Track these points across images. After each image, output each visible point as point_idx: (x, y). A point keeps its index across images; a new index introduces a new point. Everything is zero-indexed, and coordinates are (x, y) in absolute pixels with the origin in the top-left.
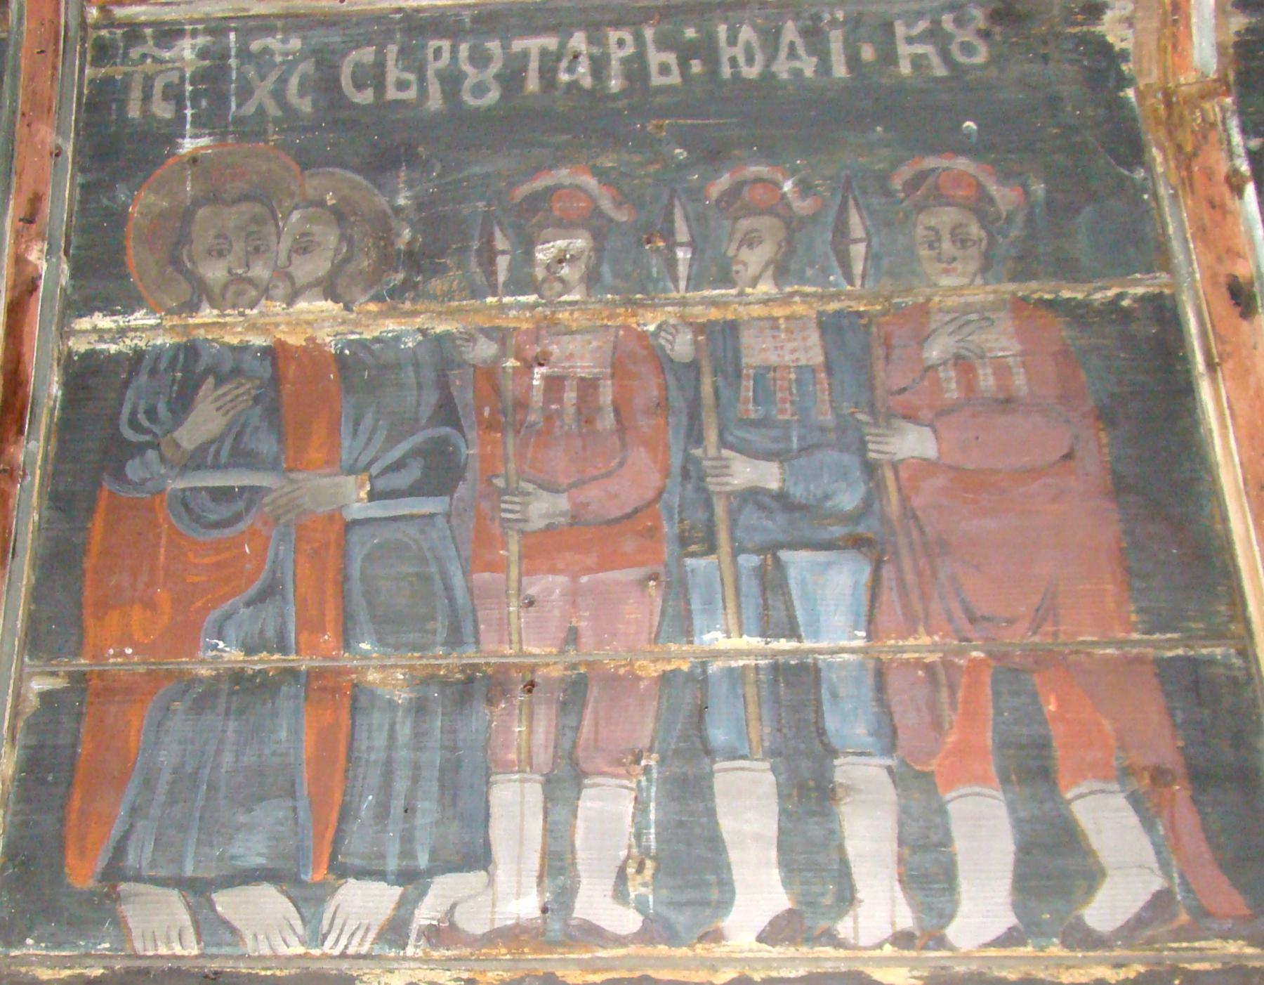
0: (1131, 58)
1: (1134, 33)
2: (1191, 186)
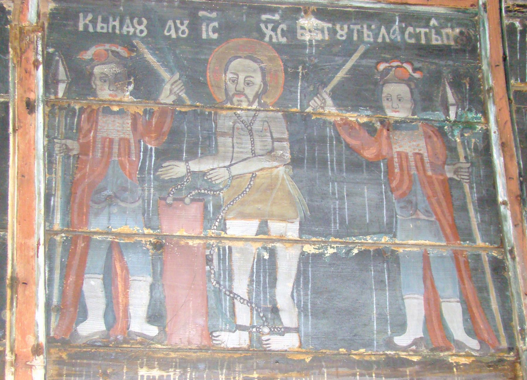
0: (12, 14)
1: (14, 5)
2: (21, 63)
